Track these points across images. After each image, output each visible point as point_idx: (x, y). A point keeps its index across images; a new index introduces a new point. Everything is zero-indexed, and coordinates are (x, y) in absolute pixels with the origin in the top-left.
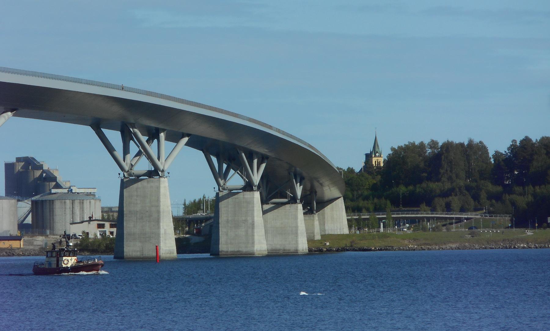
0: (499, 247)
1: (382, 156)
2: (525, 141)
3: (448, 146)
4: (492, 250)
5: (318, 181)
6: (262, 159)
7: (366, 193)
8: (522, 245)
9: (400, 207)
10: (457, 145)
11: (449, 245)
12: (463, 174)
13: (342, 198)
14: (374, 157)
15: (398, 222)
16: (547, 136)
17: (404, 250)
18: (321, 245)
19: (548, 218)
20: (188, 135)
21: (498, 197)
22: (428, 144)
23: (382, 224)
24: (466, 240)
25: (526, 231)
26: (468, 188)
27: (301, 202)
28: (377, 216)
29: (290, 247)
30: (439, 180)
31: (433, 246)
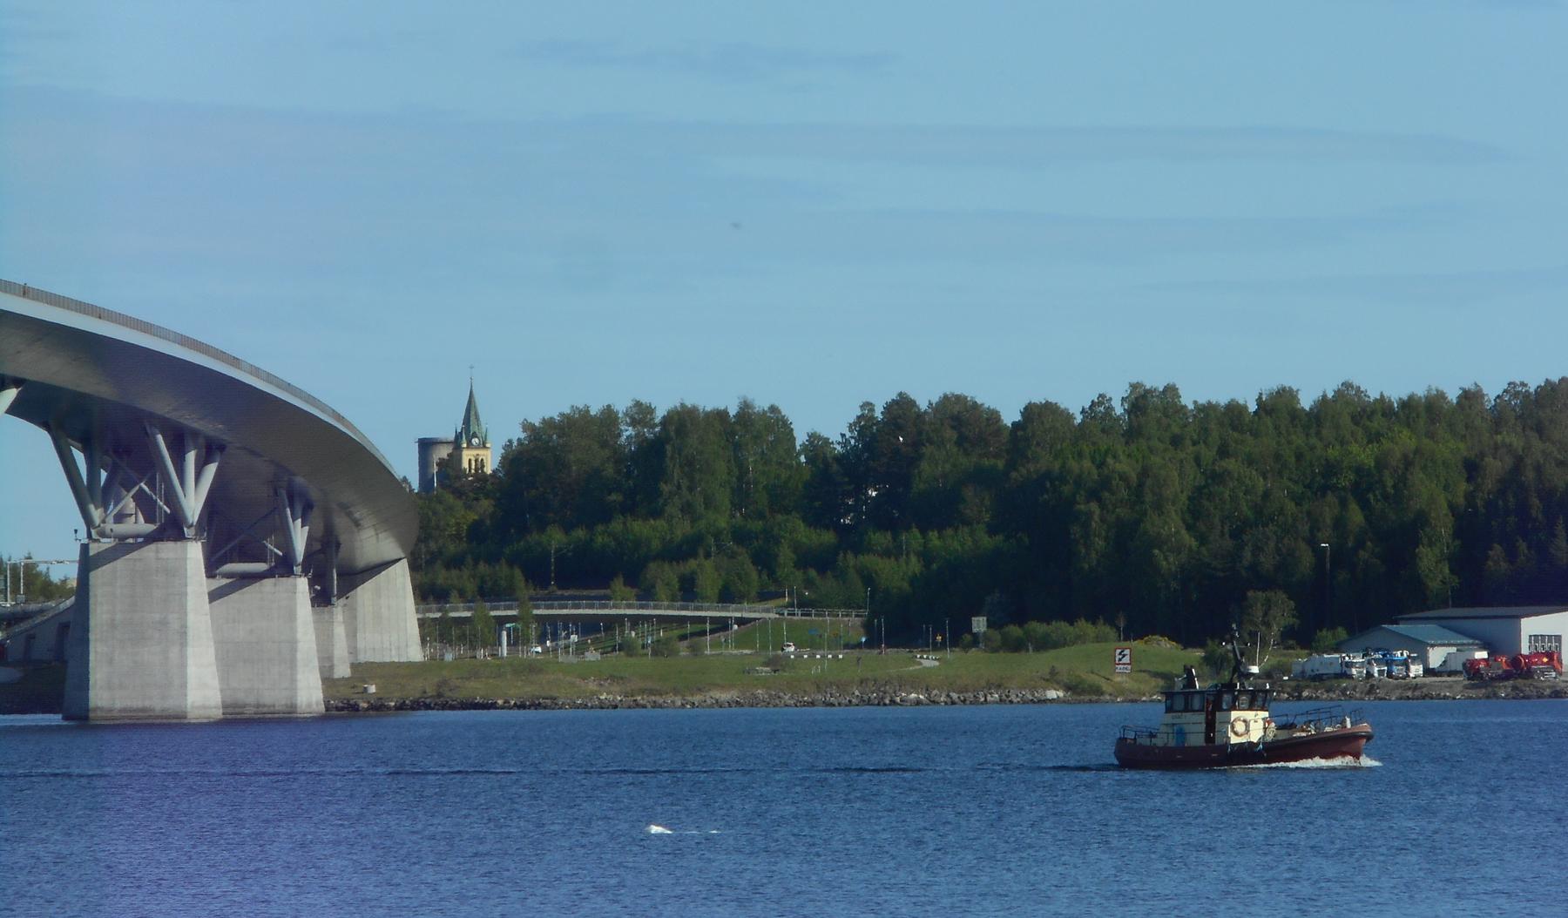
0: (850, 701)
1: (488, 445)
2: (896, 407)
3: (683, 421)
4: (828, 708)
5: (349, 514)
6: (210, 451)
7: (452, 548)
8: (913, 695)
9: (551, 589)
10: (708, 415)
11: (712, 694)
12: (723, 498)
13: (404, 563)
14: (468, 447)
15: (550, 629)
16: (957, 392)
17: (586, 706)
18: (354, 693)
19: (973, 618)
20: (17, 382)
21: (822, 562)
22: (626, 414)
23: (505, 633)
24: (757, 680)
25: (918, 656)
26: (741, 537)
27: (305, 572)
28: (493, 613)
29: (272, 696)
30: (657, 514)
31: (668, 696)
